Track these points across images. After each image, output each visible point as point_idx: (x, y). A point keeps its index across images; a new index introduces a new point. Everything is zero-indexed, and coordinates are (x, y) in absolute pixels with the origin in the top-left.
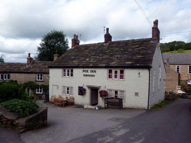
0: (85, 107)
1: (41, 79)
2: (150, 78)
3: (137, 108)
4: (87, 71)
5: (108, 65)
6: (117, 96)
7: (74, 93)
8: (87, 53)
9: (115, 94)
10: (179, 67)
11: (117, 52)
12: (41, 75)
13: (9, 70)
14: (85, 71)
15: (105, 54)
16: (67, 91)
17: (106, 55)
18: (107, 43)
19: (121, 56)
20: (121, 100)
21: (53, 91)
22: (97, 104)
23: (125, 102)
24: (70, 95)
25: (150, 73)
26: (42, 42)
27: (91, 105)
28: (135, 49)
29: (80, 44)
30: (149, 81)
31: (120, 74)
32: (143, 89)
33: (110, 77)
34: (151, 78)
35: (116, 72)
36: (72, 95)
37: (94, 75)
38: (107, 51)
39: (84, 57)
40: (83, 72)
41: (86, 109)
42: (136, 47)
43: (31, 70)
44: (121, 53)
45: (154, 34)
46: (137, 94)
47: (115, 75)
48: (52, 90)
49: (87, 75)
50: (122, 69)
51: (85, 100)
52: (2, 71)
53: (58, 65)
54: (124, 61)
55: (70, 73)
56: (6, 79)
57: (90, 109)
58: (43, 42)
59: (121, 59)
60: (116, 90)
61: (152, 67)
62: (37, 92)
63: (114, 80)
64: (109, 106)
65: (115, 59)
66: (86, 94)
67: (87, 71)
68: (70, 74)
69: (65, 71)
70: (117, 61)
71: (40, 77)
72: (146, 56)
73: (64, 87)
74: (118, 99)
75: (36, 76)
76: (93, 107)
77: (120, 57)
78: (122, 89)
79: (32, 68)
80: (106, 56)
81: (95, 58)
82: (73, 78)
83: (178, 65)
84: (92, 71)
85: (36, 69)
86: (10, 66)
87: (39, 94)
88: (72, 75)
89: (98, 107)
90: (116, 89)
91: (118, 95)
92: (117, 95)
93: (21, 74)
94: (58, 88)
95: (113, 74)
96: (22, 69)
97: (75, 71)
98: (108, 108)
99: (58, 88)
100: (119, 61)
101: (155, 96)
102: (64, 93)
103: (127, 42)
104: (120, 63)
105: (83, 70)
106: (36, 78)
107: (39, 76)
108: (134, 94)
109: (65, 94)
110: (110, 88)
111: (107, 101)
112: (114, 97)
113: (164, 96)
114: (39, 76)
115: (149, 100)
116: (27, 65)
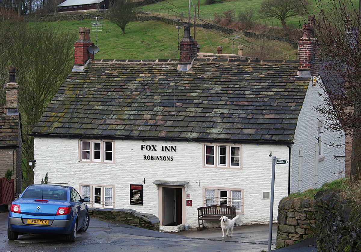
2: (291, 164)
4: (152, 148)
6: (226, 202)
16: (94, 196)
17: (193, 105)
18: (187, 64)
19: (231, 111)
28: (261, 93)
33: (210, 160)
38: (192, 94)
40: (142, 149)
44: (228, 103)
45: (305, 56)
49: (152, 158)
53: (58, 131)
54: (240, 126)
61: (293, 143)
69: (86, 145)
72: (284, 116)
74: (229, 208)
76: (175, 229)
82: (114, 163)
92: (226, 199)
95: (217, 155)
97: (118, 146)
100: (228, 125)
104: (231, 132)
105: (142, 146)
112: (219, 203)
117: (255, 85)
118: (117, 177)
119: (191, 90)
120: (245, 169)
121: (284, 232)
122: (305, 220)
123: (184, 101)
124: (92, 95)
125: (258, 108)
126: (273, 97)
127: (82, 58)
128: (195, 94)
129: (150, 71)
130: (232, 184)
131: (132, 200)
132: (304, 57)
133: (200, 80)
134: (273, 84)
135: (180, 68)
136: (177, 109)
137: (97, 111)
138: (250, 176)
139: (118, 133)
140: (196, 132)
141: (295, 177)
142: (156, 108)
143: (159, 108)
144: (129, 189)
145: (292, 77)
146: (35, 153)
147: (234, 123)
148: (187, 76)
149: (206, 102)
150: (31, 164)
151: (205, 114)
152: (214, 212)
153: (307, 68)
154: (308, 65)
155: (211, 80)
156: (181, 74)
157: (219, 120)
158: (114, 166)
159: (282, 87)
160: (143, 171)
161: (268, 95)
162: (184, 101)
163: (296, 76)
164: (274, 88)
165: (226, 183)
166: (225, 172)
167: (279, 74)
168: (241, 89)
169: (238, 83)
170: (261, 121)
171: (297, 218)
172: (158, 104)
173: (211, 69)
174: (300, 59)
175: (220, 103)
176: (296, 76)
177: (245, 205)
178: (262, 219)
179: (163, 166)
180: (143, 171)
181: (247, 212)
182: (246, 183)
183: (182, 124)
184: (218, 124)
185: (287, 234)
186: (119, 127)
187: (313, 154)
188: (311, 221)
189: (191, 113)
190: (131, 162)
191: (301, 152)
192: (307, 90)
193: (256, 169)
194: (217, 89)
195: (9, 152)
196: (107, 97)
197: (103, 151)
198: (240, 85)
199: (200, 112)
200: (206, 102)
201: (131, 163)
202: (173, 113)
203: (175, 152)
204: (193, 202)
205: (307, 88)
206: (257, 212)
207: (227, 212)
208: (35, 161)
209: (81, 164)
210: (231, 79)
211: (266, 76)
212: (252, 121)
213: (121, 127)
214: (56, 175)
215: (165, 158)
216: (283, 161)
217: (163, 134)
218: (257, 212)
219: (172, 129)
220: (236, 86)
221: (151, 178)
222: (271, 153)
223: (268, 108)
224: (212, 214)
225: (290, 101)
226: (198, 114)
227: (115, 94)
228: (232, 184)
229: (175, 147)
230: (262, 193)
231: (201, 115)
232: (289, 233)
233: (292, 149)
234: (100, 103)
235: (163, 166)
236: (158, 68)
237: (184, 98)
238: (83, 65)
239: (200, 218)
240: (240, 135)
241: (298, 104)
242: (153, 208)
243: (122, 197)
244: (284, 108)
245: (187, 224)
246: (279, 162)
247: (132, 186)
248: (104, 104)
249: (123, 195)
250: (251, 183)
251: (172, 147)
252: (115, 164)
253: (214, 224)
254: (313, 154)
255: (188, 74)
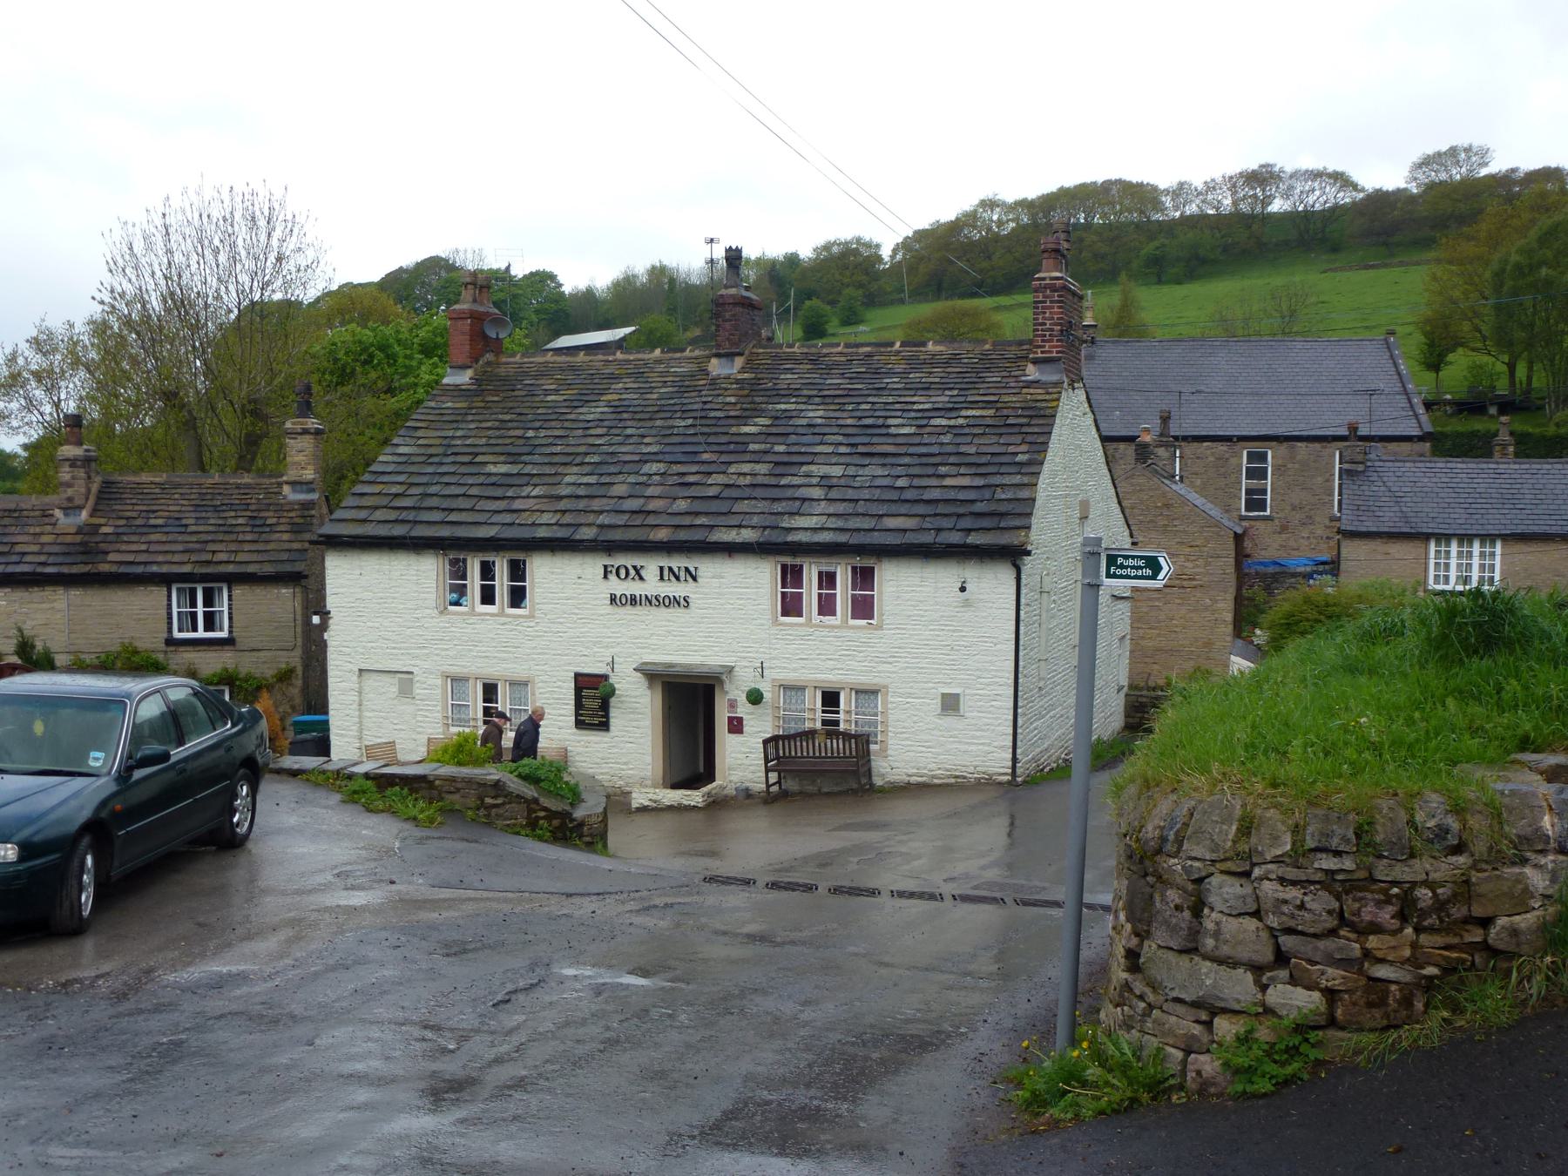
0: (639, 799)
1: (210, 623)
2: (1022, 613)
3: (953, 781)
4: (632, 572)
6: (836, 723)
9: (823, 712)
10: (1263, 458)
11: (818, 439)
15: (739, 448)
16: (480, 705)
17: (748, 457)
19: (851, 471)
20: (862, 742)
23: (884, 750)
27: (665, 787)
28: (933, 422)
32: (985, 675)
33: (791, 606)
34: (1026, 613)
35: (828, 580)
38: (746, 429)
39: (587, 469)
40: (605, 577)
41: (643, 809)
43: (111, 557)
44: (843, 449)
45: (1048, 322)
46: (950, 704)
49: (633, 601)
51: (624, 760)
57: (670, 808)
58: (155, 304)
60: (830, 687)
61: (1028, 553)
63: (818, 626)
65: (817, 493)
69: (459, 572)
72: (997, 480)
73: (457, 680)
74: (847, 736)
75: (169, 606)
76: (695, 797)
78: (866, 680)
80: (746, 468)
82: (531, 616)
83: (1257, 447)
90: (830, 677)
92: (838, 712)
93: (36, 594)
95: (810, 590)
97: (544, 572)
98: (784, 795)
100: (841, 508)
101: (1053, 707)
105: (605, 567)
111: (778, 758)
112: (818, 725)
113: (1121, 709)
115: (1019, 731)
117: (914, 403)
118: (539, 654)
119: (743, 419)
120: (890, 629)
121: (1178, 1000)
122: (1333, 932)
123: (723, 448)
124: (484, 440)
125: (924, 460)
126: (966, 431)
127: (468, 347)
128: (753, 429)
129: (638, 375)
130: (853, 670)
131: (581, 715)
132: (1045, 324)
133: (768, 393)
134: (962, 399)
135: (716, 367)
136: (703, 468)
137: (493, 479)
138: (905, 648)
139: (542, 533)
140: (753, 527)
141: (1031, 650)
142: (646, 468)
143: (654, 467)
144: (573, 685)
145: (1014, 380)
146: (329, 590)
147: (857, 501)
148: (735, 386)
149: (781, 448)
150: (316, 620)
151: (779, 478)
152: (805, 750)
153: (1054, 355)
154: (1057, 347)
155: (796, 393)
156: (718, 381)
157: (817, 493)
158: (532, 624)
159: (987, 405)
160: (610, 637)
161: (950, 426)
162: (723, 448)
163: (1023, 378)
164: (966, 408)
165: (838, 669)
166: (835, 637)
167: (978, 373)
168: (877, 414)
169: (870, 399)
170: (935, 494)
171: (1273, 921)
172: (652, 457)
173: (797, 366)
174: (1035, 330)
175: (819, 449)
176: (1023, 378)
177: (890, 729)
178: (939, 769)
179: (664, 623)
180: (610, 637)
181: (896, 750)
182: (894, 669)
183: (715, 506)
184: (814, 503)
185: (1204, 1016)
186: (546, 518)
187: (1069, 588)
188: (1368, 945)
189: (741, 478)
190: (577, 611)
191: (1047, 580)
192: (1056, 412)
193: (920, 630)
194: (811, 414)
195: (284, 591)
196: (522, 442)
197: (502, 583)
198: (873, 403)
199: (765, 475)
200: (781, 448)
201: (577, 614)
202: (691, 479)
203: (694, 584)
204: (745, 722)
205: (1058, 406)
206: (923, 749)
207: (841, 751)
208: (329, 612)
209: (444, 618)
210: (850, 389)
211: (943, 381)
212: (909, 495)
213: (551, 519)
214: (382, 648)
215: (667, 601)
216: (1141, 563)
217: (662, 535)
218: (923, 749)
219: (687, 521)
220: (863, 407)
221: (630, 657)
222: (964, 582)
223: (952, 459)
224: (799, 755)
225: (1013, 439)
226: (759, 480)
227: (542, 435)
228: (853, 670)
229: (696, 568)
230: (940, 697)
231: (766, 480)
232: (1215, 1012)
233: (1025, 570)
234: (502, 458)
235: (664, 623)
236: (661, 368)
237: (724, 439)
238: (470, 367)
239: (771, 766)
240: (876, 534)
241: (1036, 448)
242: (637, 738)
243: (554, 709)
244: (997, 460)
245: (731, 781)
246: (1122, 567)
247: (580, 678)
248: (512, 460)
249: (558, 704)
250: (908, 667)
251: (687, 569)
252: (533, 617)
253: (805, 782)
254: (1069, 588)
255: (737, 381)
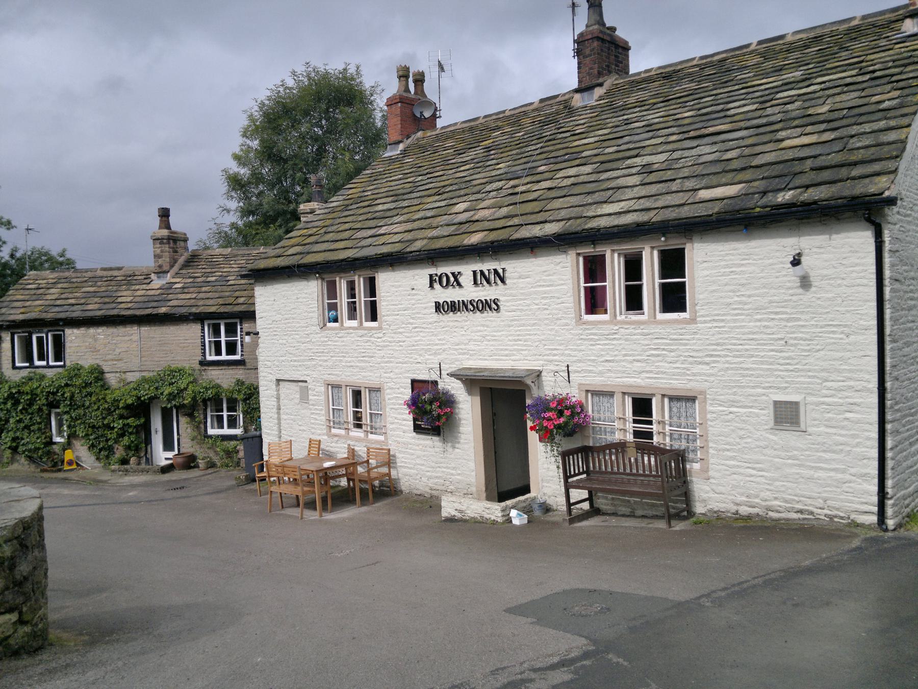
0: (449, 508)
1: (231, 348)
4: (452, 279)
5: (574, 226)
6: (649, 435)
7: (389, 419)
8: (467, 167)
9: (635, 421)
11: (651, 134)
12: (226, 325)
13: (57, 309)
14: (444, 279)
16: (351, 409)
21: (279, 413)
22: (526, 489)
24: (371, 436)
25: (887, 246)
26: (248, 142)
27: (489, 498)
29: (440, 123)
30: (874, 312)
31: (658, 281)
34: (892, 290)
36: (382, 438)
37: (495, 302)
40: (431, 286)
41: (451, 520)
42: (788, 85)
47: (664, 288)
48: (275, 410)
49: (453, 307)
50: (673, 243)
52: (21, 317)
55: (362, 298)
56: (44, 363)
59: (669, 175)
62: (216, 424)
64: (602, 502)
66: (458, 426)
67: (452, 279)
68: (362, 309)
69: (332, 292)
70: (644, 191)
71: (223, 339)
73: (336, 387)
74: (658, 451)
75: (204, 336)
76: (494, 511)
77: (664, 166)
78: (680, 385)
79: (183, 290)
80: (572, 172)
81: (504, 192)
82: (380, 328)
84: (480, 278)
85: (202, 295)
86: (65, 285)
87: (225, 438)
88: (374, 317)
89: (527, 510)
91: (655, 427)
93: (121, 330)
94: (304, 396)
96: (129, 299)
99: (304, 396)
102: (338, 424)
103: (725, 60)
105: (431, 276)
106: (204, 345)
107: (217, 332)
108: (770, 411)
109: (343, 432)
110: (597, 381)
112: (630, 437)
114: (217, 332)
115: (889, 454)
116: (153, 276)
160: (437, 345)
177: (711, 445)
206: (754, 472)
218: (754, 472)
